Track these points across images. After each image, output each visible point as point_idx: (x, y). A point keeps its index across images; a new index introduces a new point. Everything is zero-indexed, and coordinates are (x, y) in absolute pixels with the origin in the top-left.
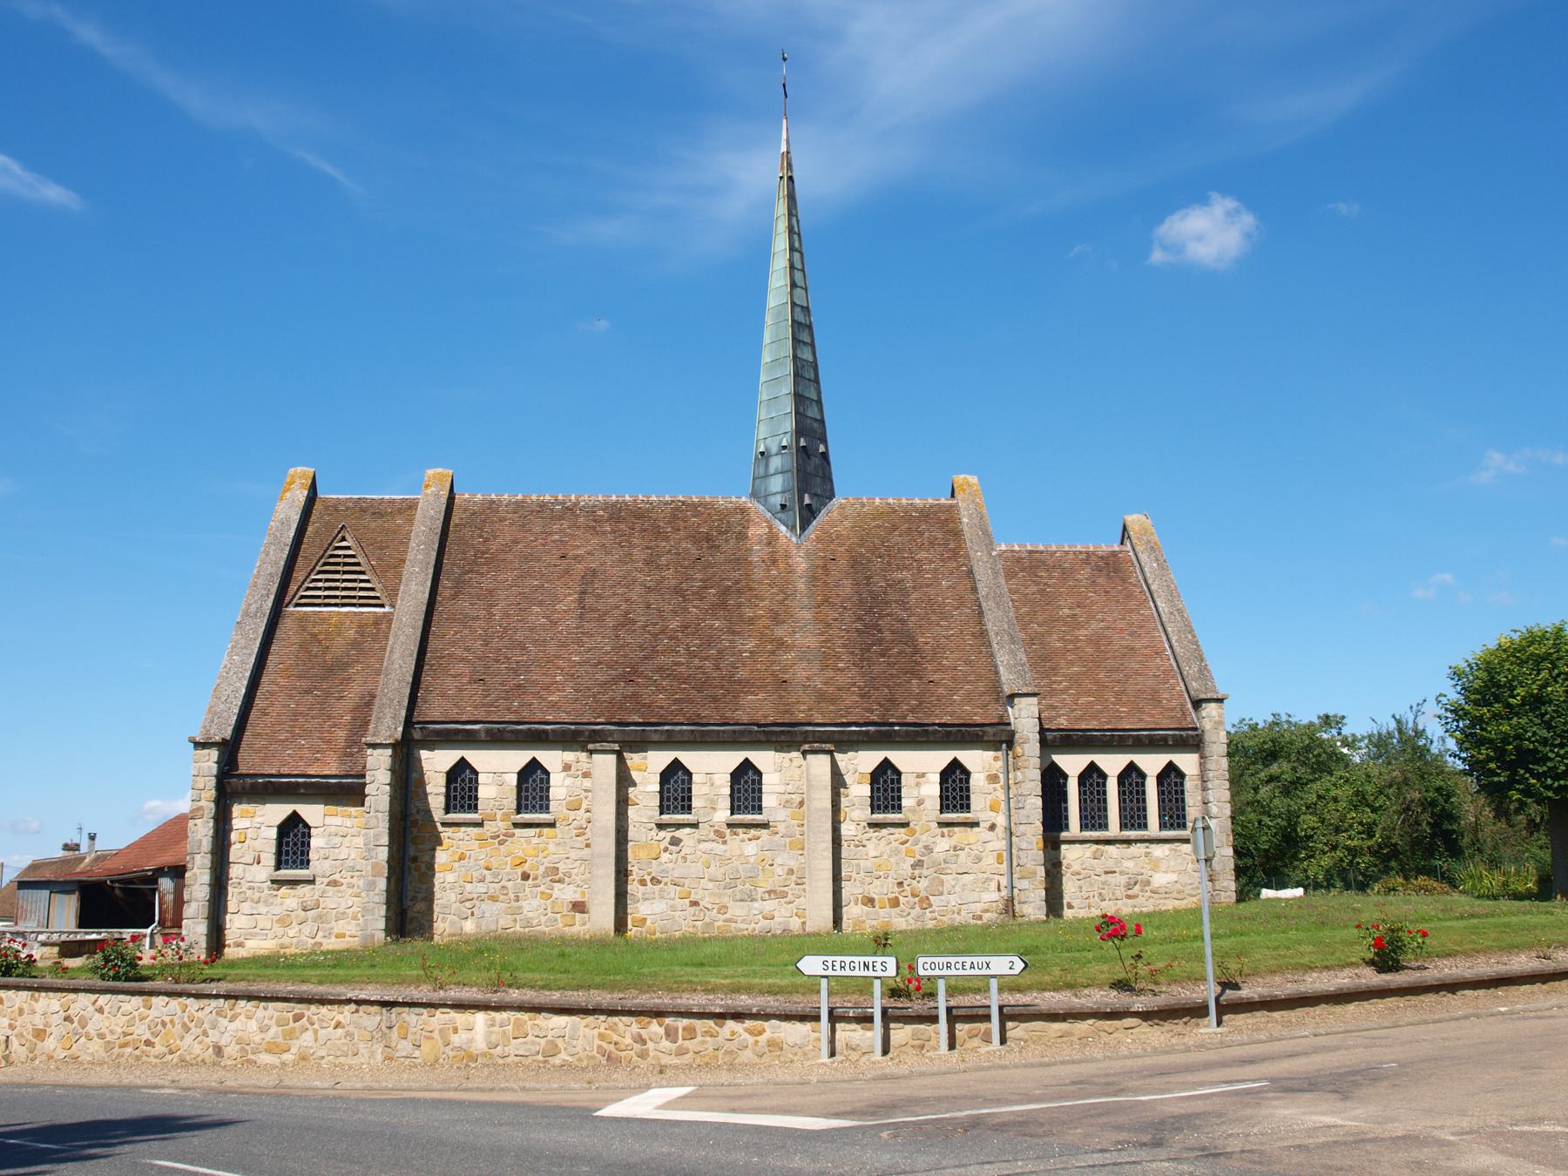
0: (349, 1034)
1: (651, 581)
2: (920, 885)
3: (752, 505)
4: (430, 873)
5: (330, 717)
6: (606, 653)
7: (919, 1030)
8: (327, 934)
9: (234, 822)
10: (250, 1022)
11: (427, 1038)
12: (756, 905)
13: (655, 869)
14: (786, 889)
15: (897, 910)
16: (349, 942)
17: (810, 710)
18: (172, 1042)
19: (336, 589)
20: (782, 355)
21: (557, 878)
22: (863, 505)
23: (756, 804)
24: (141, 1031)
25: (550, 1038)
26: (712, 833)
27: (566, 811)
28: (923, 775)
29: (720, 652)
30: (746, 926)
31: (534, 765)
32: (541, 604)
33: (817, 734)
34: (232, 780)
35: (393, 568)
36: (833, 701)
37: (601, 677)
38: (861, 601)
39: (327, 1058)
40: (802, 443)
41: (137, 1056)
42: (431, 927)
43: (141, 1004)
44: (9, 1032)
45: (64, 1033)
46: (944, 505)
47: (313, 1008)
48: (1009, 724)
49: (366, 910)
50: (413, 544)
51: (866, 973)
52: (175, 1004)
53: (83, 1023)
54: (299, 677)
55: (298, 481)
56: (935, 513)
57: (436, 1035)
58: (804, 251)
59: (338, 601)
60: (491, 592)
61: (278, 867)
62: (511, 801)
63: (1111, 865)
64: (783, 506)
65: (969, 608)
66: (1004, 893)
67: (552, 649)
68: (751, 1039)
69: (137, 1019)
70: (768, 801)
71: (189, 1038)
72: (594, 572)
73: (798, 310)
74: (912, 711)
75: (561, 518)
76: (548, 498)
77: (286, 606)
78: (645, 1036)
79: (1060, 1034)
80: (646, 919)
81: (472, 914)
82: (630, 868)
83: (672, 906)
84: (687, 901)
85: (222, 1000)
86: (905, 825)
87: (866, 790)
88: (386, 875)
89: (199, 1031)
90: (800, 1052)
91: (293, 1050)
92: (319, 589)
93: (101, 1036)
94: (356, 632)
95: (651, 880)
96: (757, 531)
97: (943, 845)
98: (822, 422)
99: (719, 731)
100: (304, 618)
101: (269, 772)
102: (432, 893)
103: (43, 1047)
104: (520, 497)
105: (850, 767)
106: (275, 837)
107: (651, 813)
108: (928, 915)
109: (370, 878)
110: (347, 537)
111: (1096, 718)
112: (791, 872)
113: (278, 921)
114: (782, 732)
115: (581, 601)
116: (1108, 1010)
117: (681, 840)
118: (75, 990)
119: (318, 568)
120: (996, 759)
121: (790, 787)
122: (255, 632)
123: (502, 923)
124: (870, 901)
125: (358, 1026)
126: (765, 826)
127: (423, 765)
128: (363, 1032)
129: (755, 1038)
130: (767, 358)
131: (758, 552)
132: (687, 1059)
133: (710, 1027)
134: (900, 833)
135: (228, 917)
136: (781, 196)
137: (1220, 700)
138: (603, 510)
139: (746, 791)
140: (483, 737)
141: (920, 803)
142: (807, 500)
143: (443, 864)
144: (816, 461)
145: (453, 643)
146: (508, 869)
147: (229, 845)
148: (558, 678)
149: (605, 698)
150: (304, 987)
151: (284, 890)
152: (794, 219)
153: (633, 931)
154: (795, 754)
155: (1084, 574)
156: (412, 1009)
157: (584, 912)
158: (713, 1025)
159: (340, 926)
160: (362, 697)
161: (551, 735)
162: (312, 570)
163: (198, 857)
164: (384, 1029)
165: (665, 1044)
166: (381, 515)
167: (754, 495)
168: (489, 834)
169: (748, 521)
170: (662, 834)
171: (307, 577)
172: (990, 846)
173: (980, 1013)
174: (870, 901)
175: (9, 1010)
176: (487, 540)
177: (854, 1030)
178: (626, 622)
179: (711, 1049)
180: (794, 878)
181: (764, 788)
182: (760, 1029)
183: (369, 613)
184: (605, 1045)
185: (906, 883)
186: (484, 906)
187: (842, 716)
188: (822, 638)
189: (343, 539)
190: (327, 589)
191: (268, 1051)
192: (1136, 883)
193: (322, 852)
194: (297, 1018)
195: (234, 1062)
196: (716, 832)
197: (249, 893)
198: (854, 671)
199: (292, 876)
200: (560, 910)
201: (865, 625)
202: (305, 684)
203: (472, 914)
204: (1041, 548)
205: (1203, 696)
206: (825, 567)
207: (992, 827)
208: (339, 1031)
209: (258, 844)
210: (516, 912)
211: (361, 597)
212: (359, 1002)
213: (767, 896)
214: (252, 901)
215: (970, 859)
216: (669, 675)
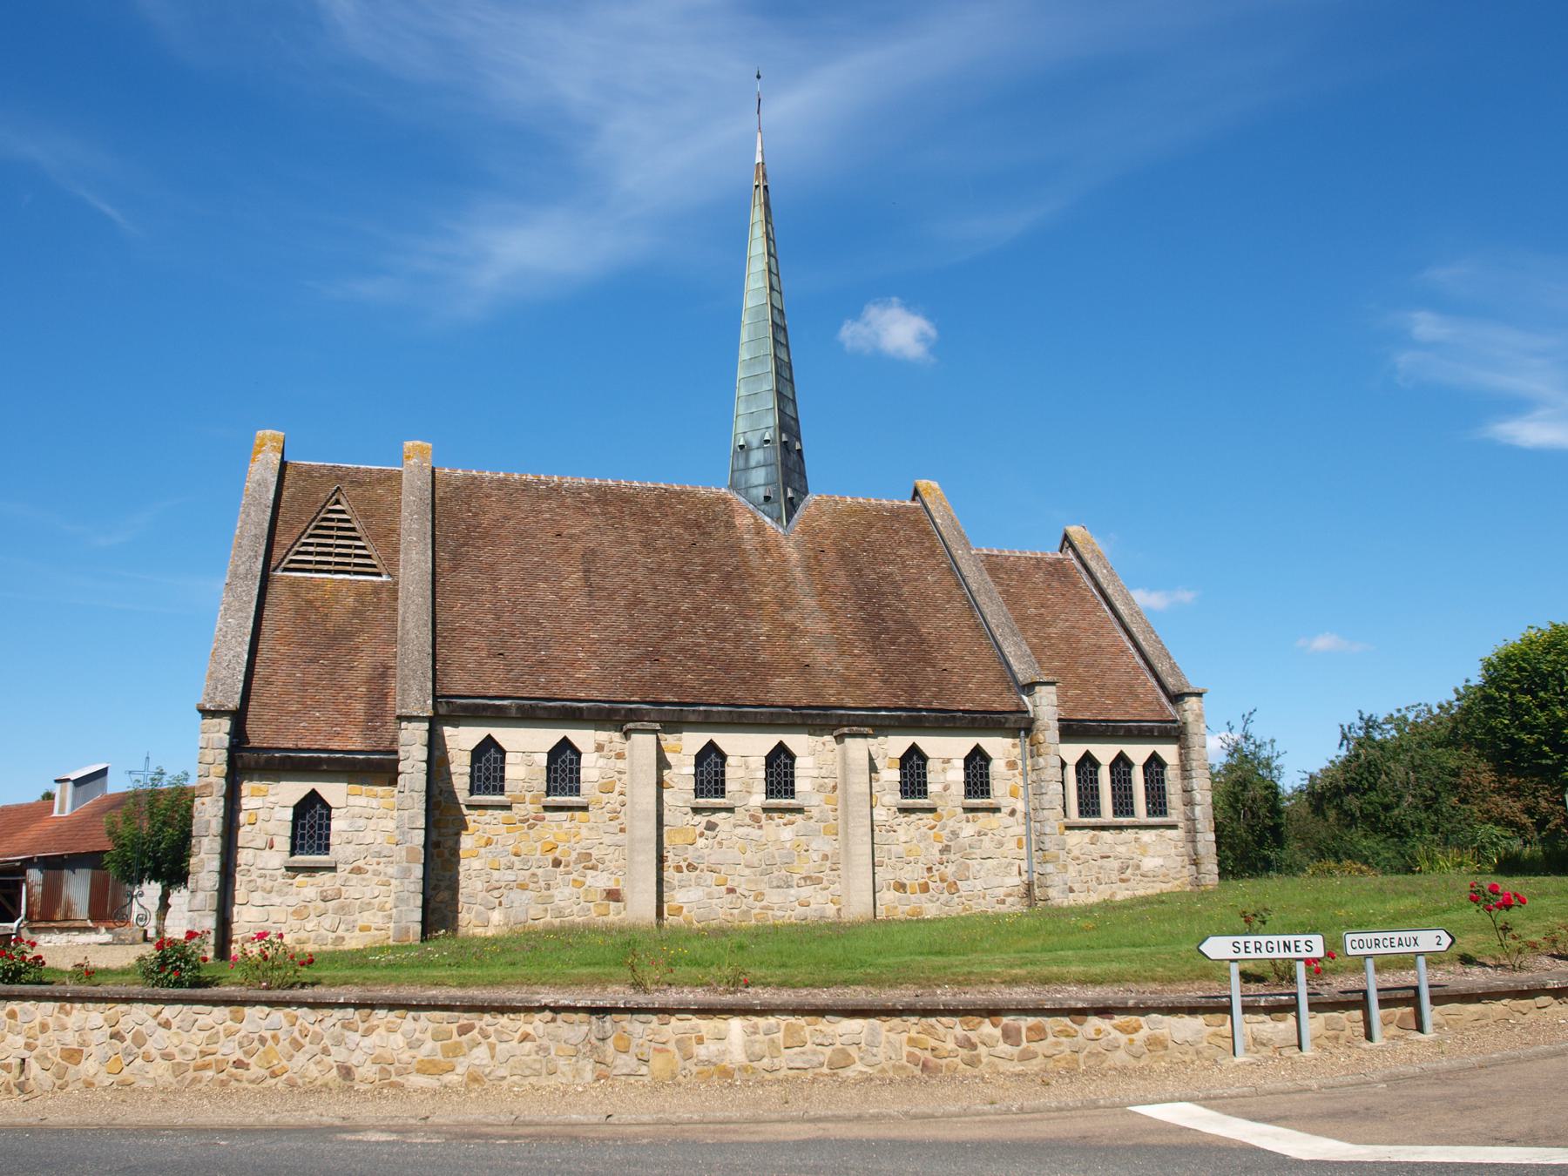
0: (541, 1049)
1: (652, 562)
2: (947, 870)
3: (732, 495)
4: (453, 859)
5: (342, 688)
6: (624, 632)
7: (1334, 1018)
8: (350, 927)
9: (243, 801)
10: (392, 1036)
11: (660, 1051)
12: (792, 891)
13: (691, 854)
14: (821, 875)
15: (927, 895)
16: (374, 936)
17: (840, 694)
18: (275, 1062)
19: (329, 554)
20: (762, 352)
21: (590, 864)
22: (837, 503)
23: (789, 788)
24: (229, 1050)
25: (838, 1045)
26: (748, 818)
27: (598, 793)
28: (948, 761)
29: (737, 634)
30: (783, 913)
31: (565, 744)
32: (546, 580)
33: (851, 718)
34: (244, 754)
35: (388, 536)
36: (859, 686)
37: (625, 655)
38: (858, 591)
39: (510, 1080)
40: (784, 438)
41: (222, 1081)
42: (455, 918)
43: (229, 1016)
44: (26, 1054)
45: (111, 1053)
46: (910, 507)
47: (487, 1017)
48: (1027, 712)
49: (400, 900)
50: (405, 513)
51: (1288, 955)
52: (279, 1016)
53: (139, 1040)
54: (302, 645)
55: (269, 444)
56: (904, 514)
57: (672, 1046)
58: (778, 257)
59: (331, 567)
60: (492, 566)
61: (292, 853)
62: (541, 782)
63: (1106, 850)
64: (767, 498)
65: (960, 602)
66: (1025, 877)
67: (568, 625)
68: (1123, 1039)
69: (222, 1034)
70: (801, 785)
71: (300, 1058)
72: (593, 551)
73: (776, 312)
74: (935, 697)
75: (548, 498)
76: (530, 477)
77: (274, 570)
78: (975, 1039)
79: (1476, 1017)
80: (682, 907)
81: (500, 904)
82: (665, 854)
83: (708, 894)
84: (723, 888)
85: (351, 1010)
86: (932, 810)
87: (895, 775)
88: (423, 861)
89: (317, 1049)
90: (1191, 1050)
91: (459, 1070)
92: (310, 553)
93: (167, 1056)
94: (355, 600)
95: (687, 867)
96: (743, 521)
97: (968, 830)
98: (796, 420)
99: (757, 713)
100: (294, 584)
101: (286, 746)
102: (457, 881)
103: (78, 1072)
104: (502, 475)
105: (881, 752)
106: (291, 818)
107: (686, 796)
108: (956, 900)
109: (405, 864)
110: (342, 500)
111: (1087, 709)
112: (825, 857)
113: (294, 913)
114: (819, 714)
115: (586, 579)
116: (1525, 988)
117: (716, 825)
118: (128, 1000)
119: (309, 531)
120: (1014, 746)
121: (824, 771)
122: (249, 594)
123: (532, 913)
124: (901, 887)
125: (556, 1039)
126: (800, 810)
127: (447, 742)
128: (564, 1046)
130: (744, 354)
131: (750, 542)
132: (1034, 1066)
133: (1067, 1025)
134: (928, 818)
135: (236, 909)
136: (757, 202)
137: (1199, 695)
138: (589, 492)
139: (779, 774)
140: (513, 712)
141: (946, 788)
142: (790, 494)
143: (469, 850)
144: (794, 456)
145: (464, 616)
146: (538, 855)
147: (238, 827)
148: (581, 655)
149: (633, 676)
150: (433, 992)
151: (300, 878)
152: (770, 226)
153: (670, 920)
154: (828, 738)
155: (1039, 577)
156: (635, 1016)
157: (618, 901)
158: (1070, 1023)
159: (366, 918)
160: (375, 669)
161: (585, 713)
162: (303, 533)
163: (205, 841)
164: (594, 1040)
165: (1003, 1048)
166: (360, 484)
167: (733, 486)
168: (517, 817)
169: (732, 510)
170: (698, 818)
171: (298, 540)
172: (1010, 831)
173: (1399, 996)
174: (901, 887)
175: (26, 1026)
176: (475, 515)
177: (1263, 1022)
178: (636, 602)
179: (1068, 1051)
180: (828, 864)
181: (797, 772)
182: (1135, 1025)
183: (365, 581)
184: (917, 1051)
185: (935, 868)
186: (512, 895)
187: (871, 700)
188: (832, 625)
189: (338, 502)
190: (318, 554)
191: (421, 1071)
192: (1128, 867)
193: (345, 835)
194: (463, 1030)
195: (369, 1087)
196: (752, 816)
197: (260, 881)
198: (870, 658)
199: (311, 862)
200: (594, 898)
201: (868, 614)
202: (309, 652)
203: (500, 904)
204: (996, 552)
205: (1186, 690)
206: (816, 558)
207: (1013, 813)
208: (528, 1045)
209: (270, 826)
210: (546, 901)
211: (356, 565)
212: (557, 1010)
213: (803, 882)
214: (264, 890)
215: (993, 844)
216: (692, 656)
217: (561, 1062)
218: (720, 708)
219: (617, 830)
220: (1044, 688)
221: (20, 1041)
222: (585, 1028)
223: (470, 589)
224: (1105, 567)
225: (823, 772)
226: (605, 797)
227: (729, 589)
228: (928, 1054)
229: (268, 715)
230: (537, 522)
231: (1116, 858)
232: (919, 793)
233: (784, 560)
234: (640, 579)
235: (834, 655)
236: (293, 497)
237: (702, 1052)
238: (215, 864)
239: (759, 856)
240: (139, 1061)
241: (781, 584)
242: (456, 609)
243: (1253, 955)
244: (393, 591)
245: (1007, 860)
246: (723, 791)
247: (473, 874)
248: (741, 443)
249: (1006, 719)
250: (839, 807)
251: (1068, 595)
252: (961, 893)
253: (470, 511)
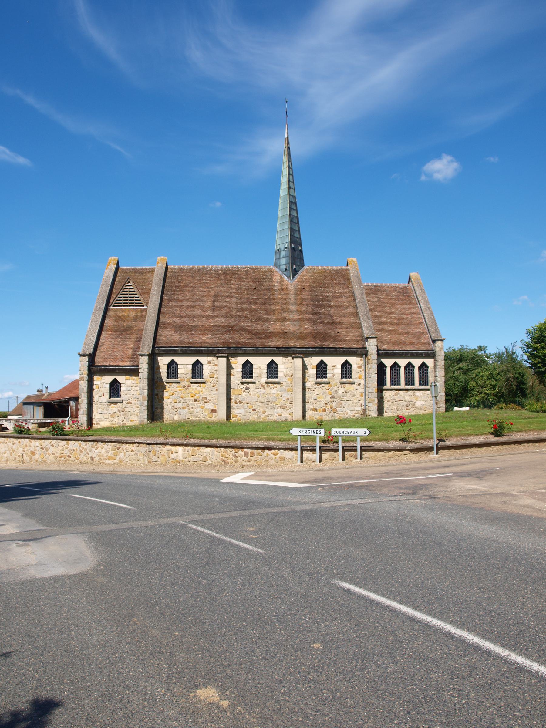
5: (126, 345)
7: (332, 454)
9: (94, 382)
12: (275, 410)
13: (240, 398)
17: (295, 342)
19: (127, 300)
20: (286, 214)
21: (206, 401)
23: (276, 375)
24: (66, 453)
25: (204, 455)
28: (335, 366)
29: (263, 322)
31: (198, 362)
36: (303, 339)
37: (221, 331)
40: (293, 246)
42: (163, 418)
43: (66, 443)
47: (123, 445)
48: (366, 348)
50: (153, 284)
51: (314, 434)
52: (77, 443)
54: (115, 332)
55: (112, 262)
57: (165, 454)
59: (127, 305)
60: (181, 301)
61: (110, 397)
63: (401, 398)
64: (286, 269)
66: (363, 407)
68: (274, 457)
70: (280, 374)
71: (82, 455)
72: (218, 293)
73: (291, 197)
75: (206, 274)
76: (201, 267)
77: (110, 307)
78: (237, 455)
81: (177, 413)
83: (246, 411)
84: (251, 409)
86: (328, 383)
87: (314, 371)
89: (86, 452)
90: (290, 461)
91: (117, 459)
92: (121, 300)
93: (53, 454)
94: (135, 315)
96: (276, 278)
97: (341, 390)
98: (300, 238)
100: (116, 311)
104: (191, 267)
105: (309, 363)
106: (109, 387)
107: (239, 379)
108: (336, 415)
109: (142, 401)
110: (130, 281)
111: (397, 346)
112: (288, 399)
113: (111, 416)
114: (285, 350)
115: (213, 304)
118: (44, 439)
119: (120, 293)
120: (361, 360)
122: (99, 316)
124: (315, 410)
125: (139, 451)
126: (279, 383)
131: (277, 286)
132: (251, 463)
134: (327, 386)
135: (94, 414)
137: (442, 340)
139: (272, 371)
140: (180, 352)
141: (334, 376)
142: (294, 267)
144: (298, 253)
146: (189, 398)
147: (93, 390)
148: (206, 331)
149: (222, 338)
151: (112, 405)
152: (290, 163)
153: (233, 419)
154: (290, 358)
155: (395, 294)
159: (132, 418)
163: (83, 394)
164: (148, 452)
165: (244, 458)
166: (142, 274)
167: (275, 265)
168: (182, 386)
170: (243, 386)
172: (358, 391)
174: (315, 410)
176: (180, 282)
178: (229, 311)
179: (260, 460)
180: (289, 401)
181: (279, 370)
184: (223, 458)
185: (328, 403)
186: (181, 411)
187: (306, 345)
188: (300, 317)
189: (129, 282)
190: (124, 300)
191: (109, 459)
193: (125, 392)
194: (118, 448)
196: (262, 385)
198: (311, 329)
202: (117, 334)
203: (177, 413)
204: (379, 285)
207: (359, 384)
209: (103, 390)
210: (192, 413)
212: (139, 443)
213: (279, 408)
214: (102, 409)
217: (140, 457)
218: (250, 349)
219: (215, 390)
220: (371, 339)
222: (146, 448)
223: (173, 309)
224: (421, 289)
225: (288, 370)
226: (211, 379)
227: (264, 305)
228: (226, 459)
229: (102, 355)
230: (200, 284)
231: (405, 401)
232: (324, 377)
233: (288, 292)
234: (233, 302)
235: (297, 328)
236: (120, 280)
237: (172, 456)
238: (86, 401)
239: (264, 399)
240: (47, 455)
241: (285, 302)
242: (166, 317)
243: (304, 434)
244: (145, 310)
245: (356, 401)
246: (252, 377)
247: (168, 404)
248: (278, 249)
249: (357, 351)
250: (293, 382)
251: (405, 301)
252: (338, 412)
253: (178, 281)
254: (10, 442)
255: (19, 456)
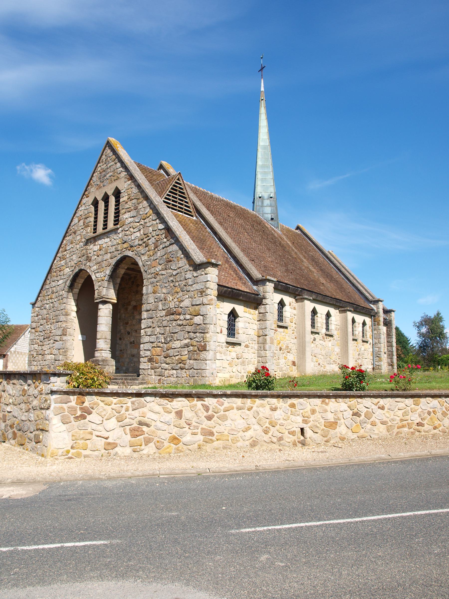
41: (412, 432)
53: (368, 416)
64: (272, 219)
93: (383, 423)
129: (153, 442)
221: (299, 419)
254: (263, 406)
255: (292, 433)
